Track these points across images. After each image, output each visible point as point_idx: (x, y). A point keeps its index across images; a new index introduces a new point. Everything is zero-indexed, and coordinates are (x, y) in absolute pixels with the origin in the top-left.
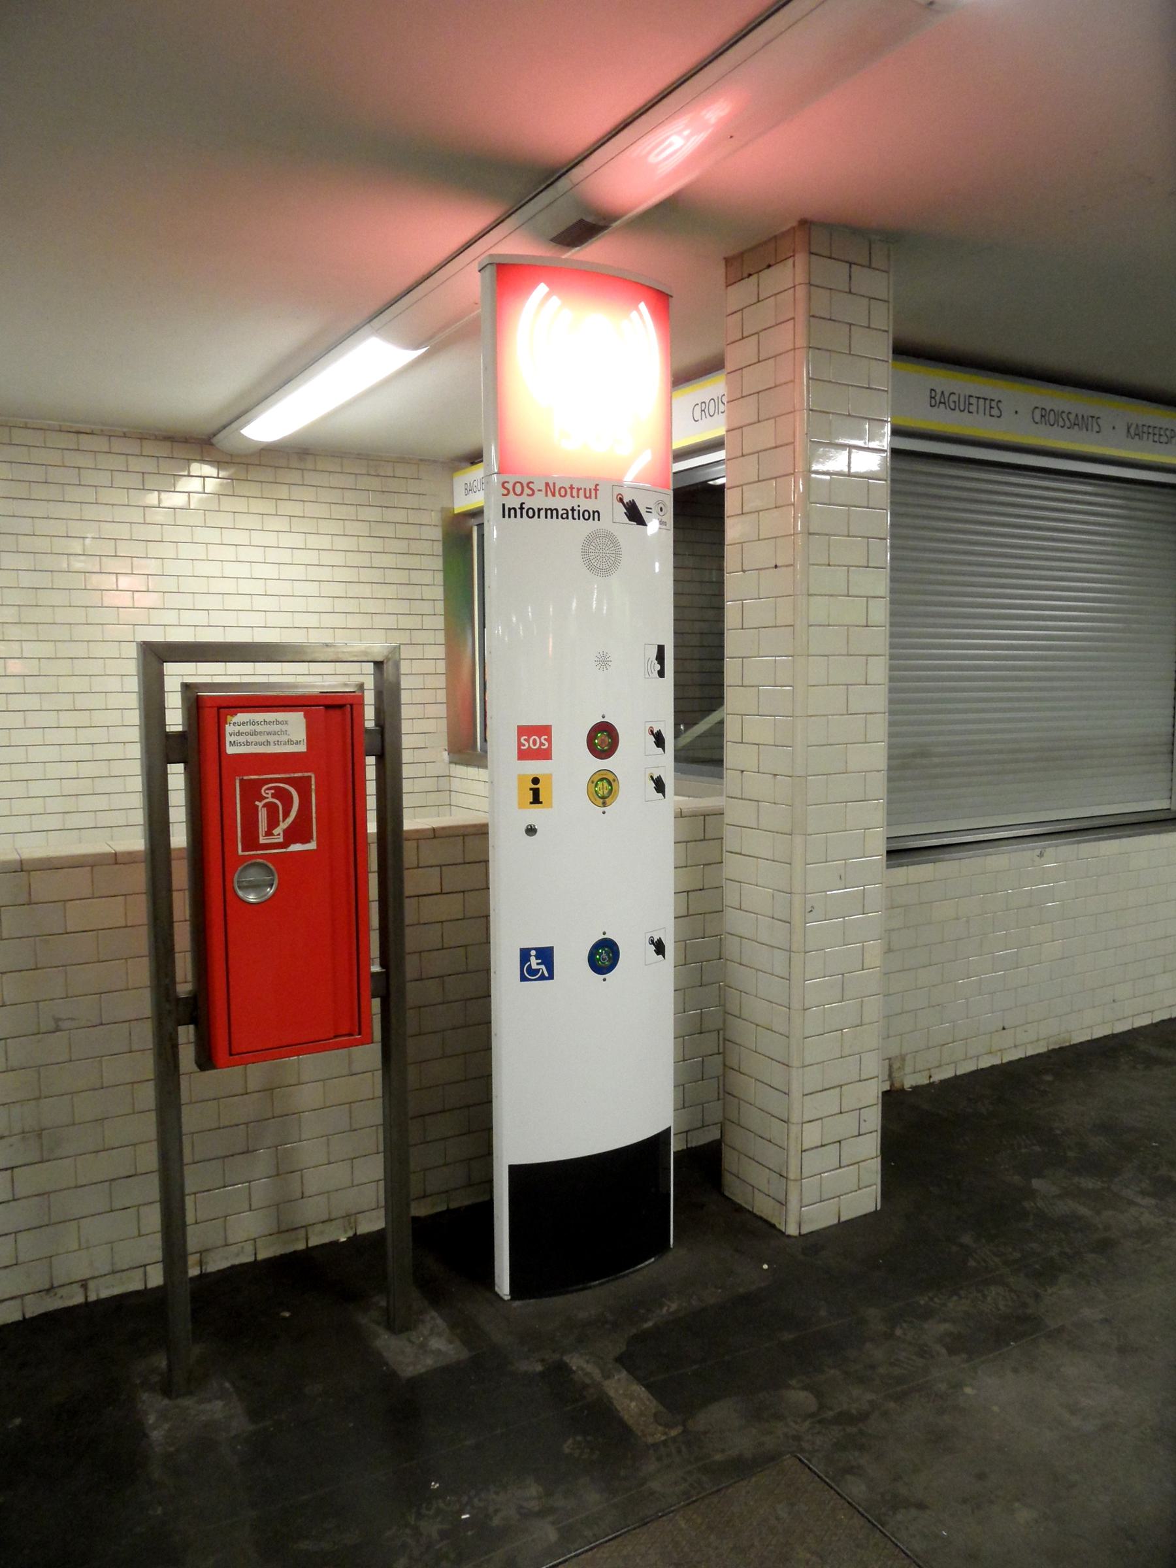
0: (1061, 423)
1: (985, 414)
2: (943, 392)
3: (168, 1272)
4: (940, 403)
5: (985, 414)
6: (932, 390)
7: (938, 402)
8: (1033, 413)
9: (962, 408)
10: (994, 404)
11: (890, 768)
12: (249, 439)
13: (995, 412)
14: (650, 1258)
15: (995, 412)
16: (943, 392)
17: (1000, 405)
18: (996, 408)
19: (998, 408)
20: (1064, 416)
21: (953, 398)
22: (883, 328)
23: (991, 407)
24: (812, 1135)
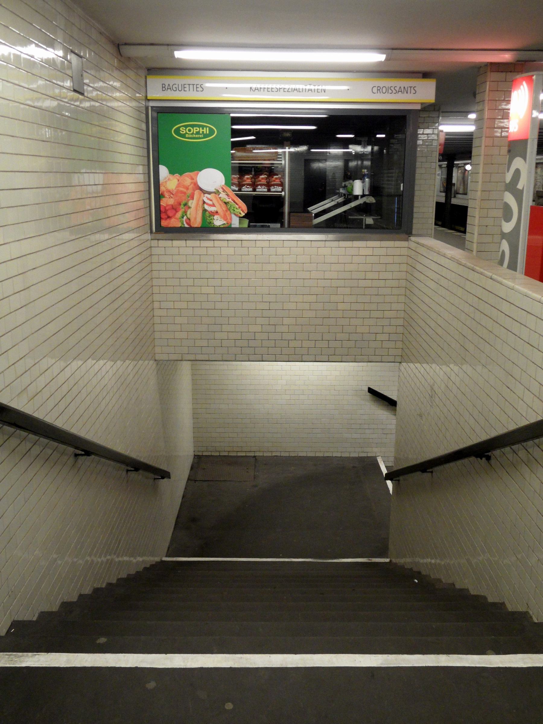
0: (390, 91)
1: (193, 91)
2: (404, 87)
3: (446, 200)
4: (168, 89)
5: (193, 91)
6: (163, 84)
7: (166, 89)
8: (372, 88)
9: (180, 89)
10: (198, 86)
11: (472, 148)
12: (174, 55)
13: (200, 89)
14: (445, 161)
15: (200, 89)
16: (404, 87)
17: (415, 88)
18: (200, 87)
19: (201, 87)
20: (392, 89)
21: (174, 86)
22: (519, 473)
23: (197, 88)
24: (419, 149)
